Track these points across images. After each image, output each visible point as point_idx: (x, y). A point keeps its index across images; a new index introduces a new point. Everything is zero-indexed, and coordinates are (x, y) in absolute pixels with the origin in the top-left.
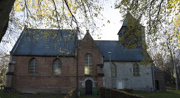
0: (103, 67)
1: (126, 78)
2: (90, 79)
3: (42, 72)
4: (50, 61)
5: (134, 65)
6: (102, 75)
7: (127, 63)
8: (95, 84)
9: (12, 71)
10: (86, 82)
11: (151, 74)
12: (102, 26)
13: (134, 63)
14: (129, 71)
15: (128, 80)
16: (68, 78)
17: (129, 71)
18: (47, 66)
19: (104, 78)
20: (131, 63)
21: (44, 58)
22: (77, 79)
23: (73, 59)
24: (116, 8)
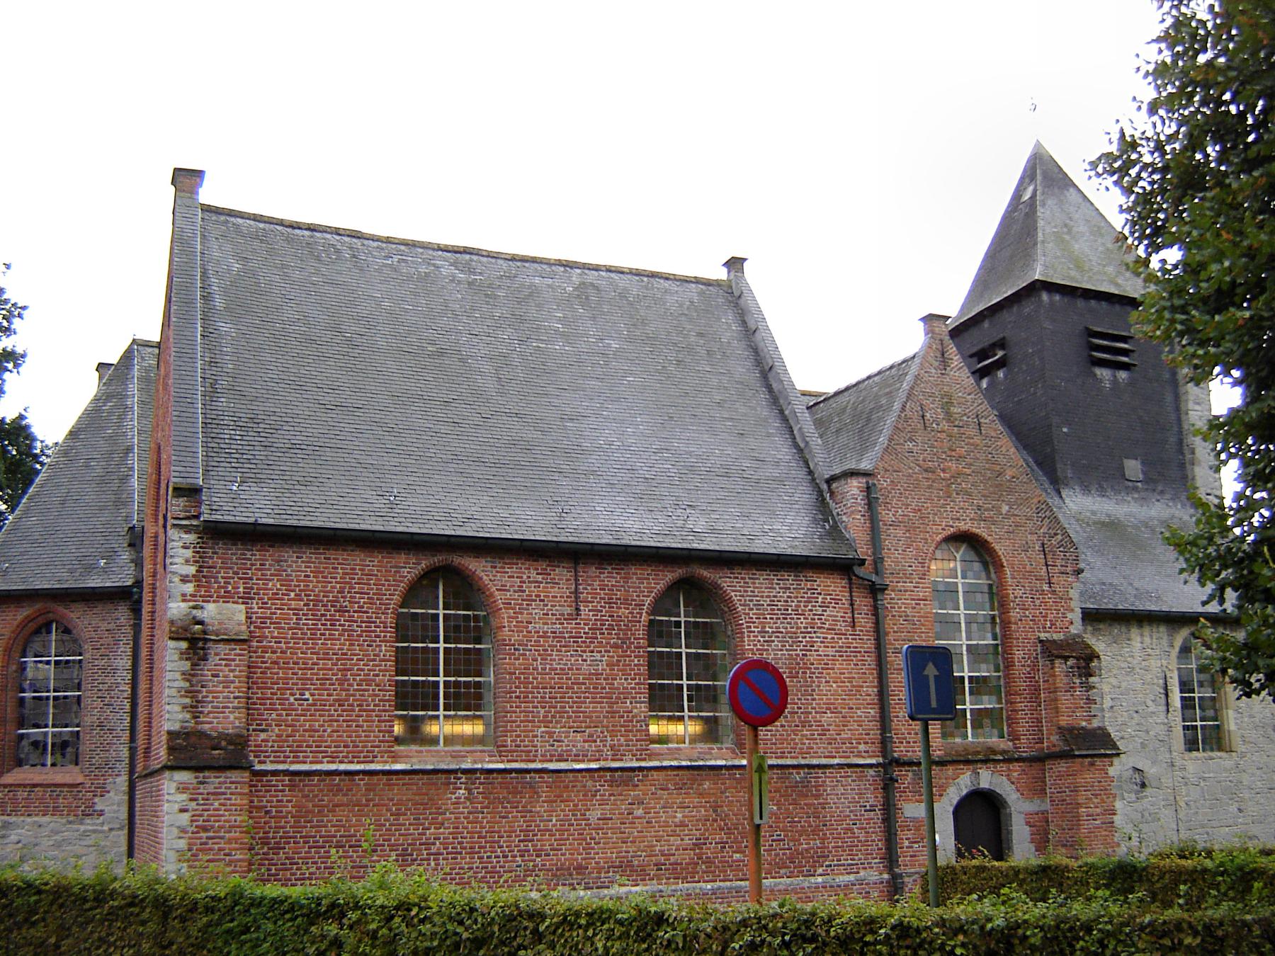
0: (1094, 664)
1: (1136, 769)
2: (987, 779)
3: (546, 723)
4: (626, 602)
5: (1185, 650)
6: (1093, 745)
7: (1134, 632)
8: (1028, 823)
9: (225, 718)
10: (956, 813)
11: (128, 688)
12: (1134, 99)
13: (1185, 633)
14: (1152, 708)
15: (1148, 791)
16: (805, 783)
17: (1152, 708)
18: (600, 661)
19: (1117, 769)
20: (1163, 629)
21: (562, 573)
22: (888, 786)
23: (831, 587)
24: (24, 308)
